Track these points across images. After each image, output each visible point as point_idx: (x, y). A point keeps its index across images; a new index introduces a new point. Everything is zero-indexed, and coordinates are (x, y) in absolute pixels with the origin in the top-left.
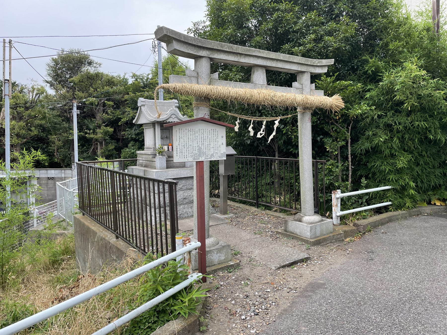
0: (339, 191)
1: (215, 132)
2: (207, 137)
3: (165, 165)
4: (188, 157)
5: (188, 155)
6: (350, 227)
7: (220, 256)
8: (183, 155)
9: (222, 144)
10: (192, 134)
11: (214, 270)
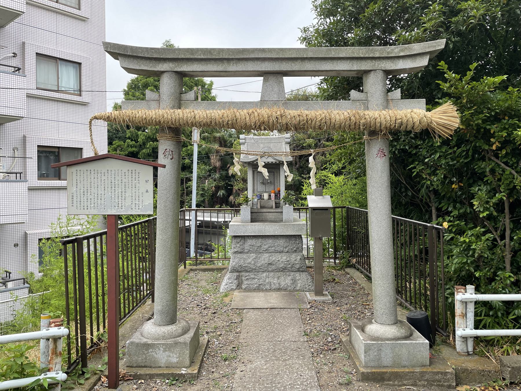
0: (471, 288)
1: (134, 174)
2: (120, 181)
3: (249, 217)
4: (89, 208)
5: (89, 206)
6: (491, 364)
7: (170, 356)
8: (82, 205)
9: (147, 191)
10: (96, 177)
11: (149, 374)
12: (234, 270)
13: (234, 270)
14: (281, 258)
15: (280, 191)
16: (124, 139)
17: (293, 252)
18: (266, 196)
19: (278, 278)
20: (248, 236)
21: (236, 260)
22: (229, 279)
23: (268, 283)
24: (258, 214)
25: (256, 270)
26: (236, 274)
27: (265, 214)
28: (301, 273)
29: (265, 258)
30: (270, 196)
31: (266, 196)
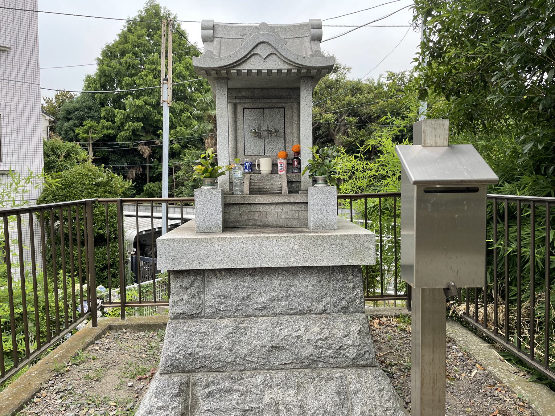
3: (218, 218)
12: (172, 369)
13: (172, 369)
14: (307, 331)
15: (298, 153)
16: (98, 119)
17: (339, 312)
18: (265, 165)
19: (299, 388)
20: (214, 271)
21: (180, 339)
22: (158, 394)
23: (270, 405)
24: (243, 208)
25: (235, 366)
26: (178, 378)
27: (261, 208)
28: (362, 371)
29: (261, 332)
30: (274, 165)
31: (265, 165)
